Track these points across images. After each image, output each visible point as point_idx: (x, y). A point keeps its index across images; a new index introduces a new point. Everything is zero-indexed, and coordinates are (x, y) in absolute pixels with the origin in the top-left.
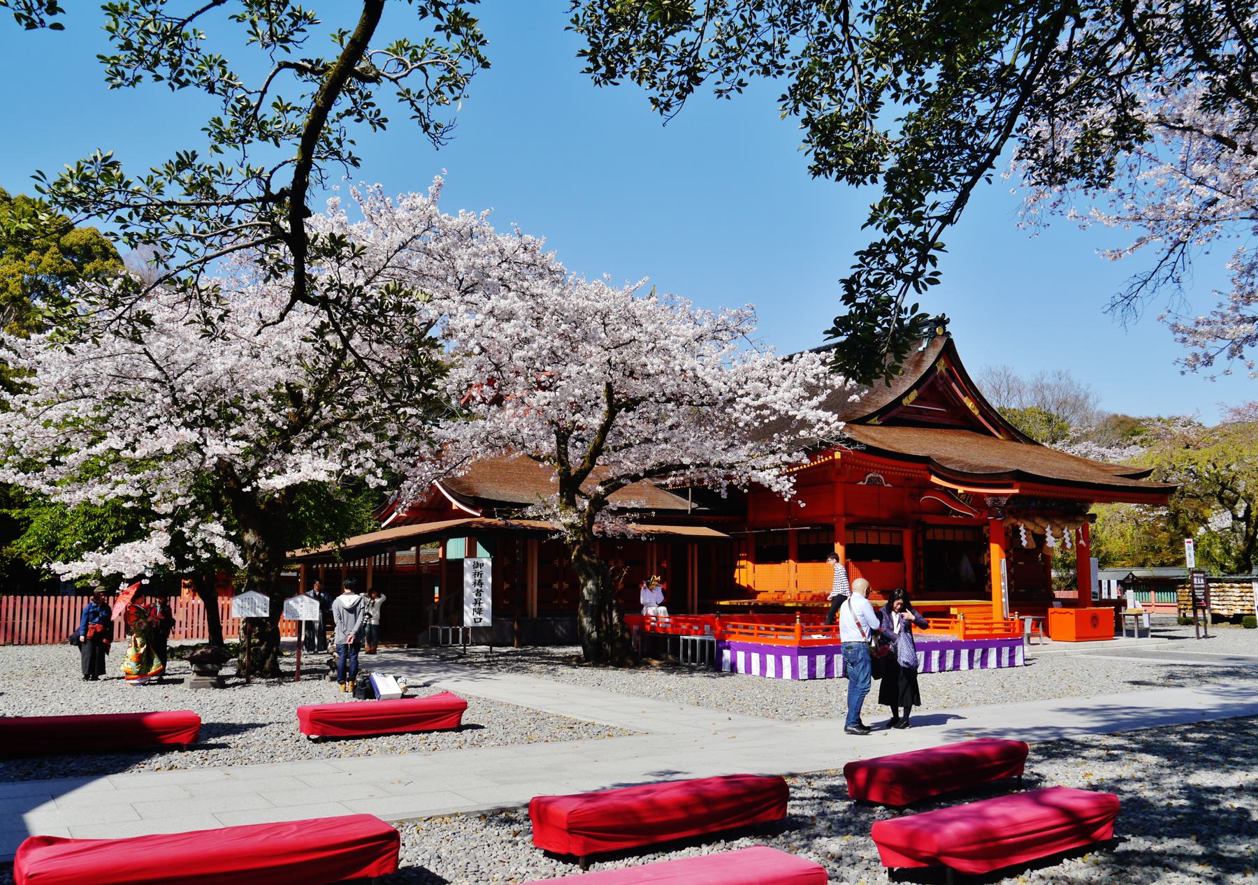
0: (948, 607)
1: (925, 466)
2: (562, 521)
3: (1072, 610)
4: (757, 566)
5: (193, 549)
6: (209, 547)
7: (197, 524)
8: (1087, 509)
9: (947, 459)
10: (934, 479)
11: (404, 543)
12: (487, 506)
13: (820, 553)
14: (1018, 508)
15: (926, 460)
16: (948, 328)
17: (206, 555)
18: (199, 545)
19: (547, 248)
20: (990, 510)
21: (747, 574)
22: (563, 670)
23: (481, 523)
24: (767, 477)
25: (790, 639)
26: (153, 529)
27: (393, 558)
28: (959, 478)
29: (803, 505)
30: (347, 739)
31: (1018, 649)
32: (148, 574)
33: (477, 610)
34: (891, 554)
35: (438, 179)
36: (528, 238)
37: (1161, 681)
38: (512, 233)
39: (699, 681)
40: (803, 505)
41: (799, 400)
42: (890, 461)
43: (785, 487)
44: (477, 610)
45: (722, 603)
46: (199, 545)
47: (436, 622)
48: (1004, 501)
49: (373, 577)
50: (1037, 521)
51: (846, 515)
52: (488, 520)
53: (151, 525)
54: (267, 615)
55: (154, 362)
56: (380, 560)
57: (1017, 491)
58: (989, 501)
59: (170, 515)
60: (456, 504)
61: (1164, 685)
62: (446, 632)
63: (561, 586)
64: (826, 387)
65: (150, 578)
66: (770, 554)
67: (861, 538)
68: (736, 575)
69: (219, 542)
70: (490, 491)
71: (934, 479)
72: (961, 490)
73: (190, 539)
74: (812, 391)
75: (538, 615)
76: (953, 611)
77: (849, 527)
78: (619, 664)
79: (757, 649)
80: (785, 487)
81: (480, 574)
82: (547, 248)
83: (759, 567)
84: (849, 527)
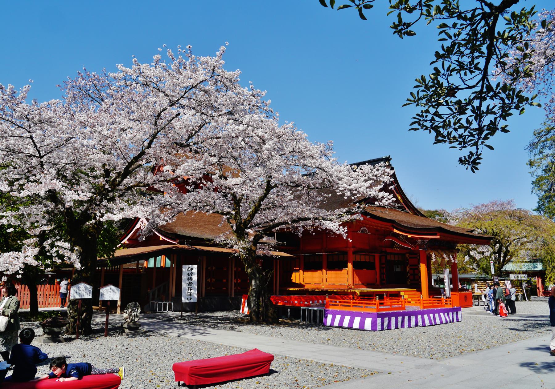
0: (399, 292)
1: (390, 224)
2: (239, 247)
4: (305, 273)
5: (51, 257)
7: (53, 242)
9: (402, 221)
11: (146, 256)
12: (181, 238)
13: (339, 266)
14: (435, 246)
15: (393, 221)
17: (59, 261)
18: (54, 255)
21: (298, 277)
22: (236, 327)
23: (178, 247)
24: (333, 226)
26: (25, 244)
28: (409, 230)
29: (351, 241)
30: (232, 381)
32: (20, 272)
33: (190, 292)
34: (370, 266)
35: (223, 48)
37: (523, 328)
39: (313, 333)
40: (351, 241)
41: (371, 187)
43: (343, 231)
44: (190, 292)
46: (54, 255)
48: (426, 242)
50: (439, 251)
51: (353, 247)
53: (24, 242)
54: (90, 297)
55: (34, 143)
56: (132, 265)
58: (419, 242)
59: (38, 236)
60: (161, 237)
61: (525, 330)
62: (165, 305)
63: (211, 280)
65: (22, 274)
66: (312, 266)
67: (358, 258)
68: (293, 278)
70: (182, 231)
72: (409, 236)
73: (49, 251)
74: (377, 183)
75: (205, 295)
76: (402, 293)
77: (355, 253)
78: (268, 323)
79: (349, 314)
80: (343, 231)
81: (189, 274)
83: (329, 272)
84: (355, 253)
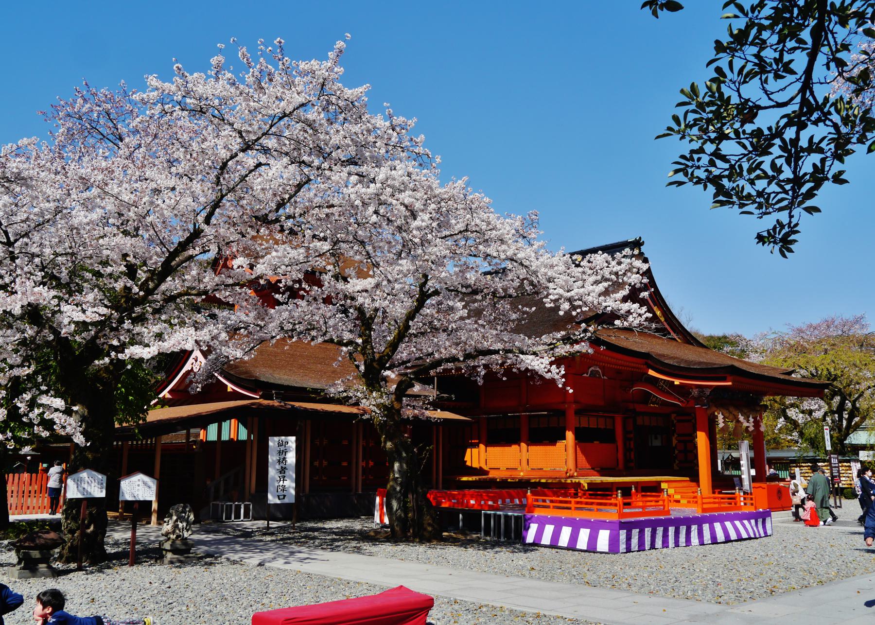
0: (659, 483)
2: (371, 404)
3: (764, 485)
6: (48, 424)
8: (761, 400)
9: (663, 356)
10: (651, 373)
13: (547, 435)
15: (646, 356)
16: (643, 249)
19: (417, 130)
20: (697, 400)
21: (477, 456)
22: (367, 546)
23: (260, 404)
24: (539, 364)
25: (611, 514)
27: (188, 435)
29: (571, 391)
31: (768, 520)
33: (282, 486)
34: (607, 436)
35: (340, 44)
36: (399, 120)
38: (383, 113)
39: (504, 557)
40: (571, 391)
41: (606, 293)
42: (620, 356)
43: (557, 374)
44: (282, 486)
45: (464, 479)
47: (216, 498)
48: (708, 392)
49: (162, 455)
50: (731, 409)
51: (575, 402)
52: (266, 402)
57: (730, 383)
60: (230, 387)
64: (624, 283)
66: (502, 436)
67: (584, 423)
68: (467, 458)
69: (59, 418)
71: (651, 373)
72: (677, 382)
75: (257, 491)
77: (578, 413)
82: (417, 130)
83: (533, 448)
84: (578, 413)
